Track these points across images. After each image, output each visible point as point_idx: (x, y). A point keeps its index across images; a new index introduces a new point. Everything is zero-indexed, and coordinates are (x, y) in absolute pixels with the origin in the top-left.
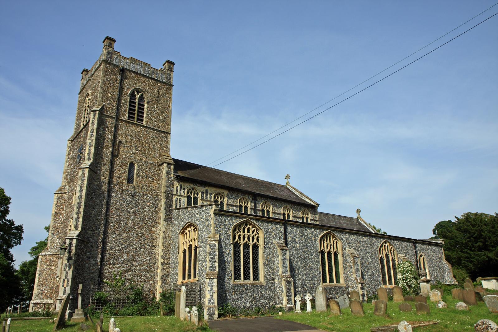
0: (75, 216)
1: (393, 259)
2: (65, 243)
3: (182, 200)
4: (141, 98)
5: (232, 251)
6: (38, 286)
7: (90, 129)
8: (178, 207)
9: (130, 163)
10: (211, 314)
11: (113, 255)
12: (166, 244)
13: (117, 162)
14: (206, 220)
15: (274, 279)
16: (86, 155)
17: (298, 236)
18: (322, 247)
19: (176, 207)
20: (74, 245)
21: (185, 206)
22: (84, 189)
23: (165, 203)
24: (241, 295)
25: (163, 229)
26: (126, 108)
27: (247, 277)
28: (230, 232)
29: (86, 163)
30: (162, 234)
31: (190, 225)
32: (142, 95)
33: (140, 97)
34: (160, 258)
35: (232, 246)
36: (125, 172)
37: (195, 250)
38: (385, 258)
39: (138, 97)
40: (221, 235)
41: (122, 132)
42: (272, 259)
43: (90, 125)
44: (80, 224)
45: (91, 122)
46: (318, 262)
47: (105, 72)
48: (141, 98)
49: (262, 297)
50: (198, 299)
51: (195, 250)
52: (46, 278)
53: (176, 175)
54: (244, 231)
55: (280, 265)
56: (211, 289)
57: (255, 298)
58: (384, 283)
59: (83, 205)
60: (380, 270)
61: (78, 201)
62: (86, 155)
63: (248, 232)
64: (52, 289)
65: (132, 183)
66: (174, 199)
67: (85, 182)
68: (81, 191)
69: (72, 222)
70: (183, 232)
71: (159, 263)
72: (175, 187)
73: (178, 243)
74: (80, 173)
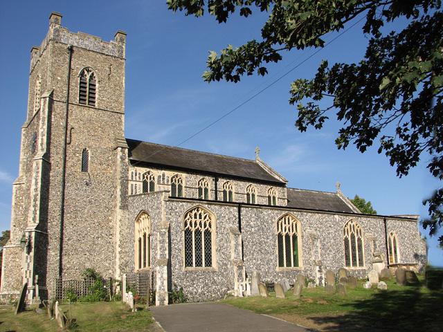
0: (33, 209)
1: (359, 240)
2: (24, 236)
3: (138, 186)
4: (92, 77)
5: (183, 238)
6: (5, 278)
7: (41, 118)
8: (134, 194)
9: (84, 150)
10: (162, 300)
11: (72, 245)
12: (123, 233)
13: (70, 150)
14: (158, 208)
15: (226, 265)
16: (39, 145)
17: (253, 219)
18: (280, 230)
19: (132, 193)
20: (33, 238)
21: (142, 192)
22: (39, 181)
23: (121, 190)
24: (193, 281)
25: (119, 217)
26: (76, 90)
27: (199, 264)
28: (181, 219)
29: (40, 154)
30: (119, 223)
31: (144, 212)
32: (93, 74)
33: (90, 76)
34: (117, 247)
35: (183, 232)
36: (79, 160)
37: (149, 238)
38: (349, 239)
39: (88, 77)
40: (171, 222)
41: (74, 117)
42: (225, 245)
43: (41, 113)
44: (38, 216)
45: (41, 110)
46: (274, 245)
47: (53, 52)
48: (92, 77)
49: (214, 282)
50: (151, 287)
51: (149, 238)
52: (11, 271)
53: (131, 160)
54: (196, 218)
55: (232, 250)
56: (162, 277)
57: (207, 285)
58: (348, 264)
59: (39, 197)
60: (344, 252)
61: (34, 193)
62: (39, 145)
63: (200, 218)
64: (18, 280)
65: (87, 171)
66: (130, 186)
67: (40, 175)
68: (36, 184)
69: (31, 215)
70: (138, 219)
71: (117, 252)
72: (130, 172)
73: (134, 231)
74: (34, 165)
